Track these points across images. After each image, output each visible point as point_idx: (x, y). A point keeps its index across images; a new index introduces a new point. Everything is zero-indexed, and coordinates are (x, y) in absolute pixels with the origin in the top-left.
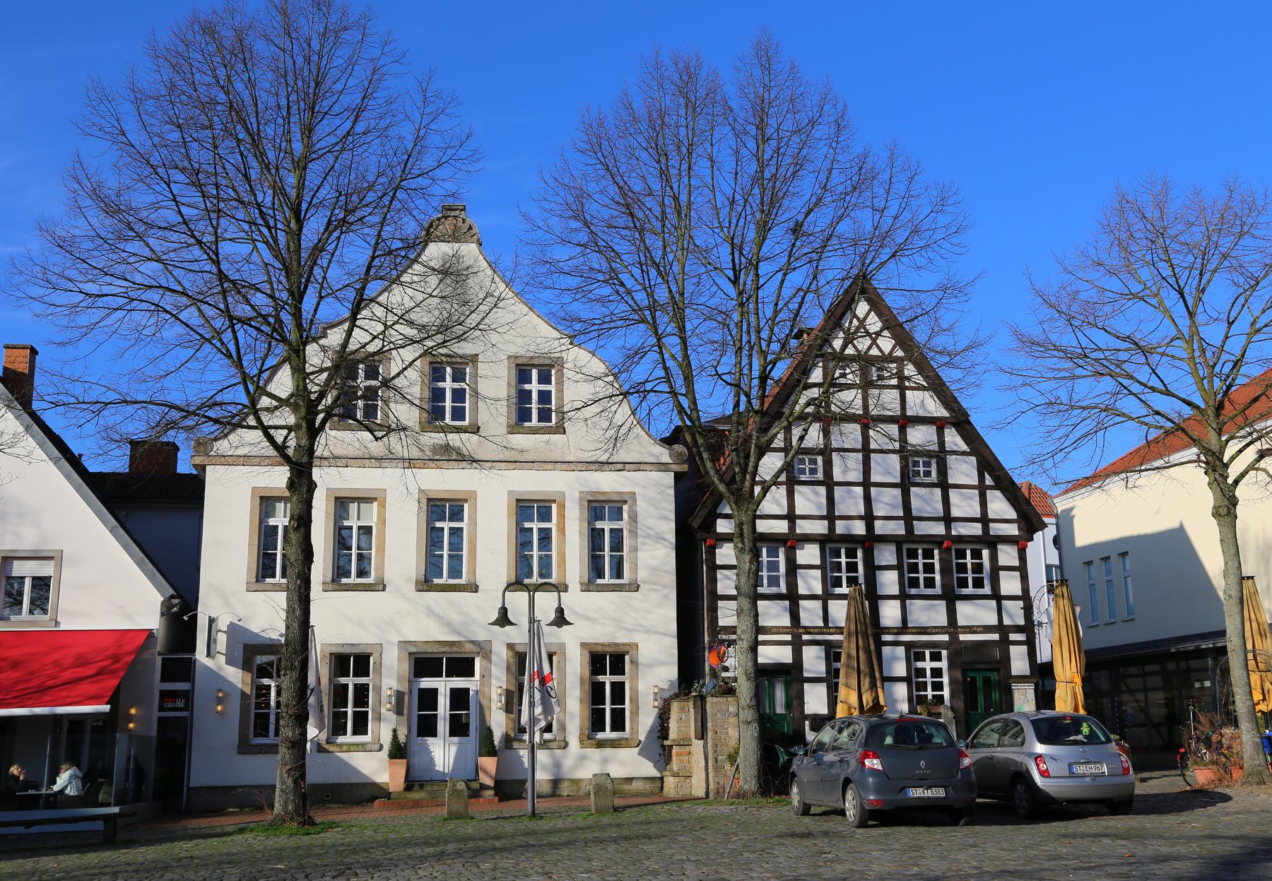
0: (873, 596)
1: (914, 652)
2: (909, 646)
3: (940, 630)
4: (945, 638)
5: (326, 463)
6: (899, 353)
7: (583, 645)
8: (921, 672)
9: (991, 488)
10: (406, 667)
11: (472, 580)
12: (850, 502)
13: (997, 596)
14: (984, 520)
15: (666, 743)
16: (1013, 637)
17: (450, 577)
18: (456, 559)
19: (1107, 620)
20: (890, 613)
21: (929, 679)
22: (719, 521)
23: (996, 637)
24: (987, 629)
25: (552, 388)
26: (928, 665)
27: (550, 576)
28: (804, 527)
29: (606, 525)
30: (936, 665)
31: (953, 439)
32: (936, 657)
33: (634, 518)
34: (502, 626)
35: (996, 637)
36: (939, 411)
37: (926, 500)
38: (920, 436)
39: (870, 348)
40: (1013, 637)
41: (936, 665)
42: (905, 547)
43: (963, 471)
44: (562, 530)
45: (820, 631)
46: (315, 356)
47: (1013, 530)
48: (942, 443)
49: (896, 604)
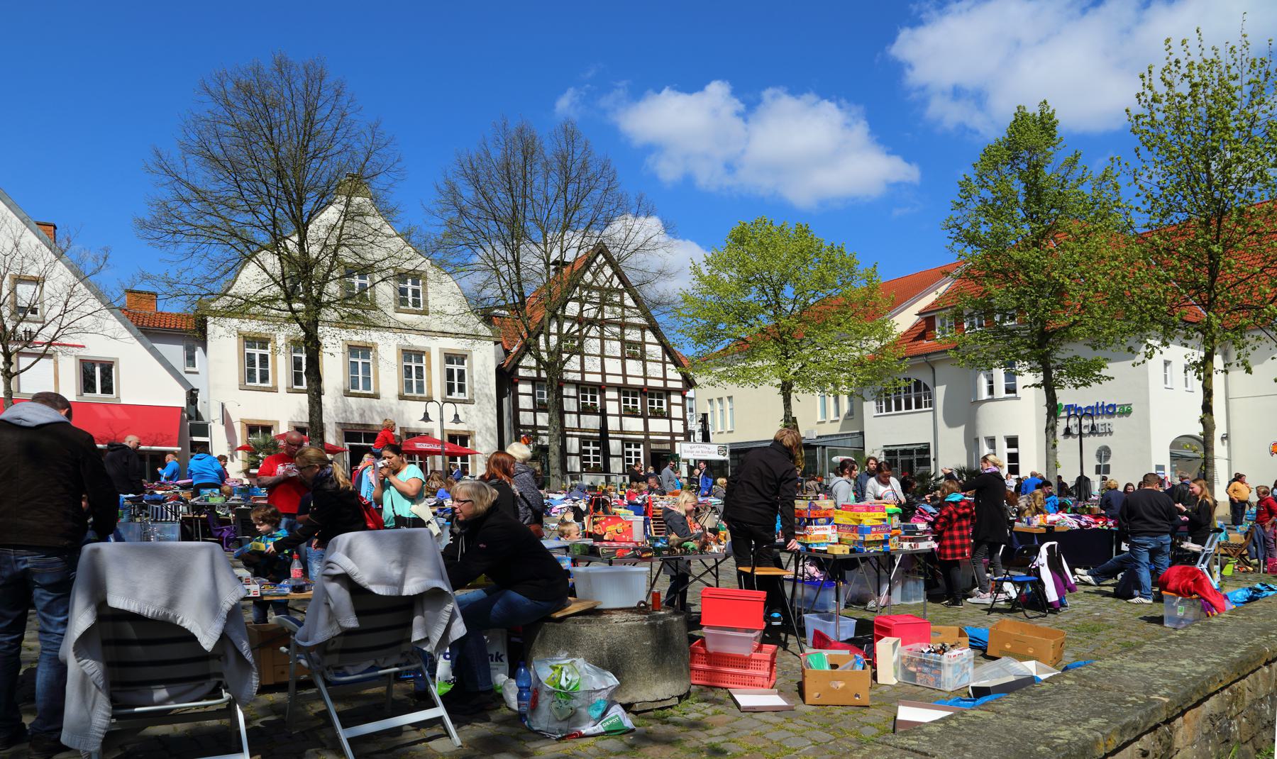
0: (562, 413)
1: (626, 443)
2: (623, 440)
3: (640, 433)
4: (643, 437)
5: (326, 323)
6: (621, 287)
7: (339, 424)
8: (629, 453)
9: (669, 363)
10: (246, 432)
11: (377, 391)
12: (592, 364)
13: (670, 418)
14: (665, 379)
15: (393, 479)
16: (677, 438)
17: (916, 408)
18: (367, 380)
19: (719, 431)
20: (570, 421)
21: (633, 457)
22: (520, 370)
23: (668, 438)
24: (664, 434)
25: (420, 288)
26: (633, 449)
27: (423, 392)
28: (609, 380)
29: (456, 367)
30: (637, 450)
31: (649, 336)
32: (637, 446)
33: (471, 366)
34: (457, 423)
35: (668, 438)
36: (641, 321)
37: (634, 367)
38: (634, 335)
39: (592, 282)
40: (677, 438)
41: (637, 450)
42: (580, 387)
43: (655, 350)
44: (429, 367)
45: (618, 432)
46: (531, 258)
47: (679, 385)
48: (643, 338)
49: (574, 416)
